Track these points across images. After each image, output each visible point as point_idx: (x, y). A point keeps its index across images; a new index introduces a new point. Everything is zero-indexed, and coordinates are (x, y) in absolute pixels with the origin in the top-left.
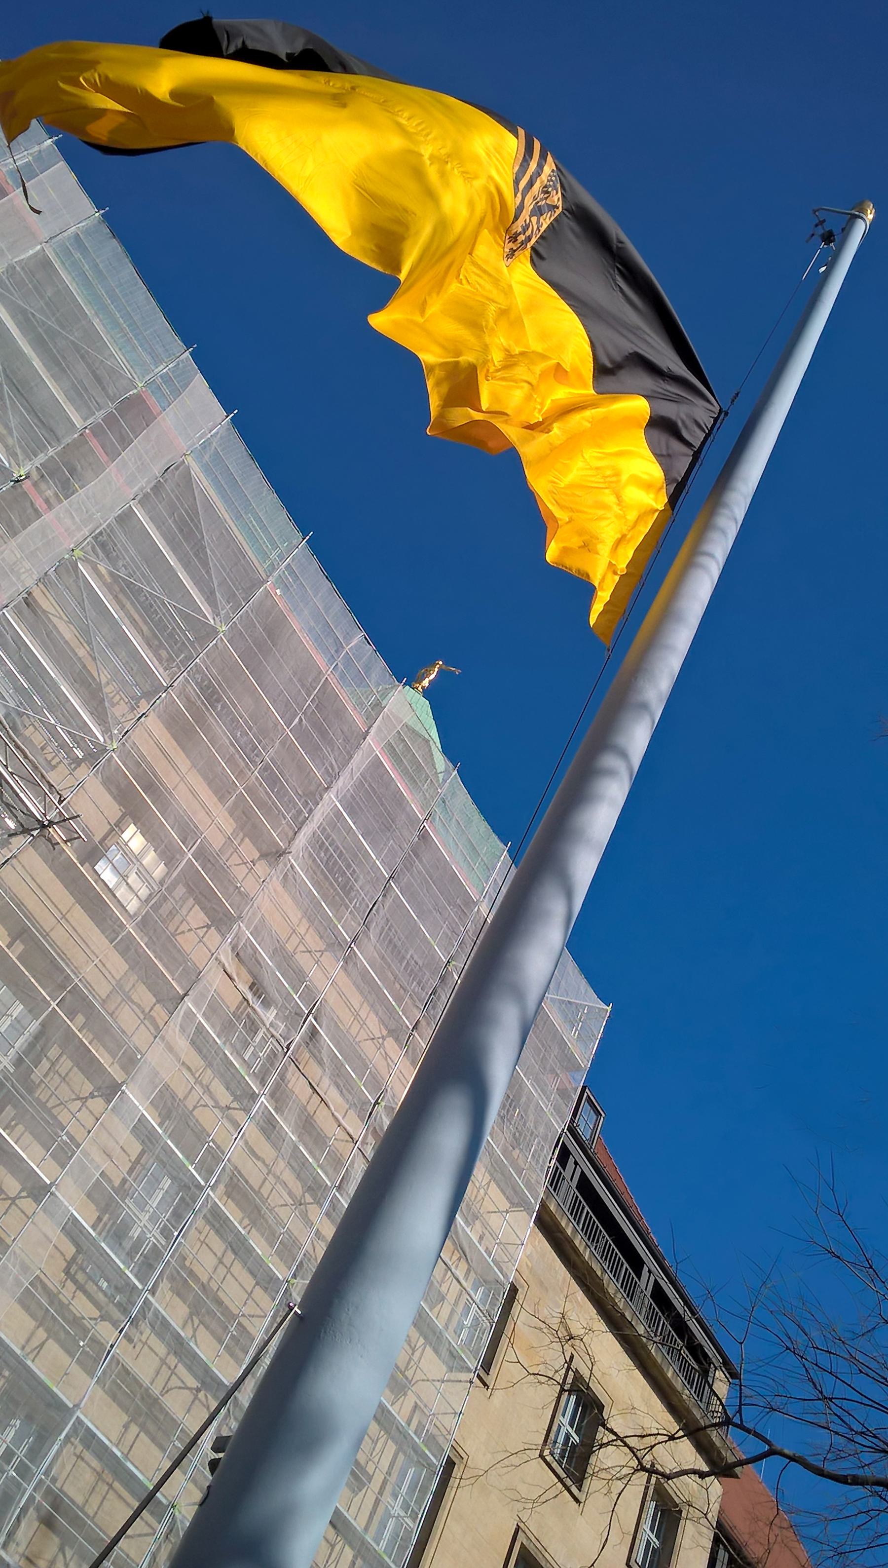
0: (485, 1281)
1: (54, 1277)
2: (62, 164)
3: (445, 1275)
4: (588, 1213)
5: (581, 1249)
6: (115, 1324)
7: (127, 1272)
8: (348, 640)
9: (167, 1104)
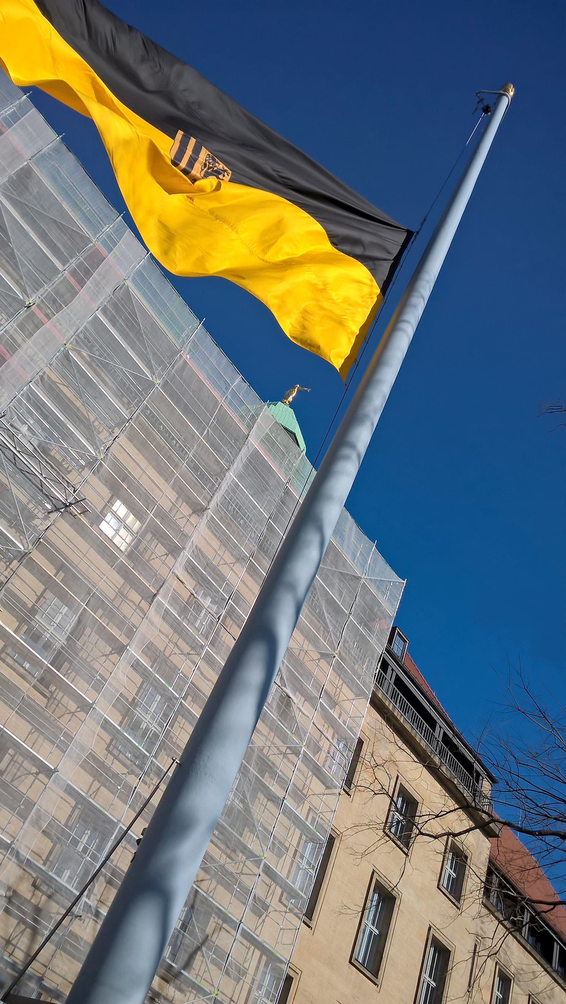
0: (343, 738)
1: (101, 753)
2: (34, 110)
3: (321, 736)
4: (401, 697)
5: (398, 717)
6: (137, 776)
7: (140, 747)
8: (233, 381)
9: (150, 650)
